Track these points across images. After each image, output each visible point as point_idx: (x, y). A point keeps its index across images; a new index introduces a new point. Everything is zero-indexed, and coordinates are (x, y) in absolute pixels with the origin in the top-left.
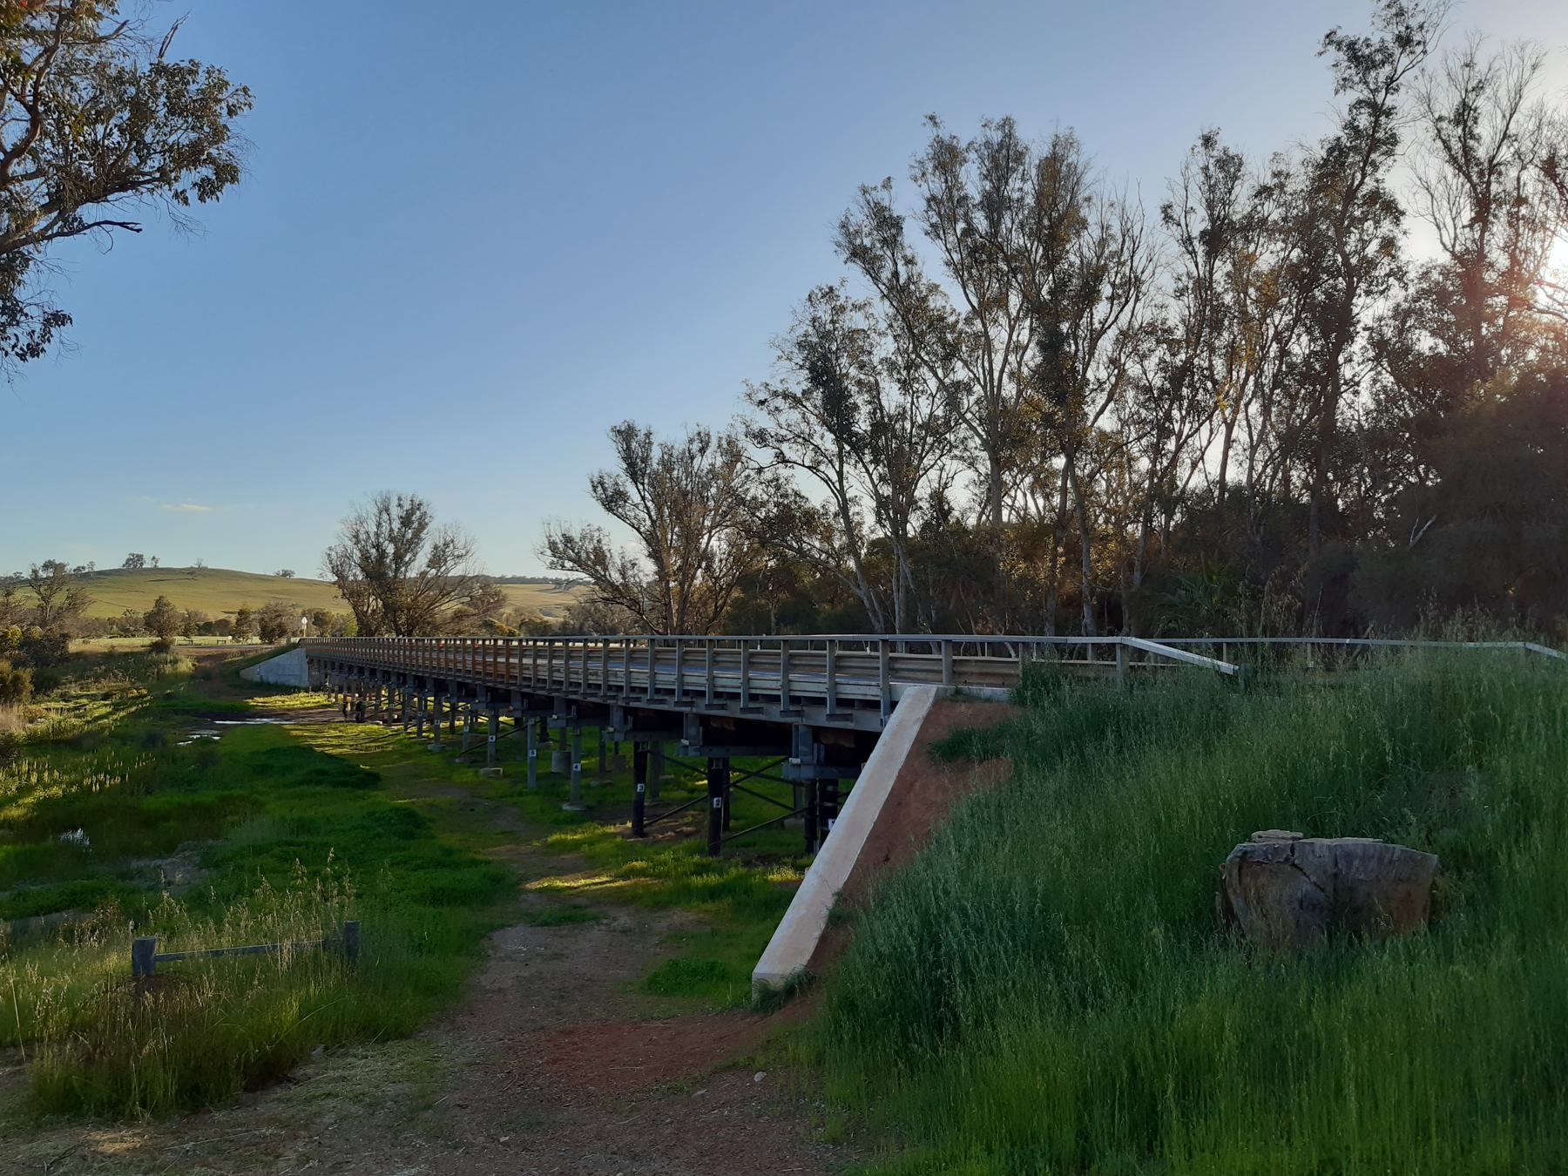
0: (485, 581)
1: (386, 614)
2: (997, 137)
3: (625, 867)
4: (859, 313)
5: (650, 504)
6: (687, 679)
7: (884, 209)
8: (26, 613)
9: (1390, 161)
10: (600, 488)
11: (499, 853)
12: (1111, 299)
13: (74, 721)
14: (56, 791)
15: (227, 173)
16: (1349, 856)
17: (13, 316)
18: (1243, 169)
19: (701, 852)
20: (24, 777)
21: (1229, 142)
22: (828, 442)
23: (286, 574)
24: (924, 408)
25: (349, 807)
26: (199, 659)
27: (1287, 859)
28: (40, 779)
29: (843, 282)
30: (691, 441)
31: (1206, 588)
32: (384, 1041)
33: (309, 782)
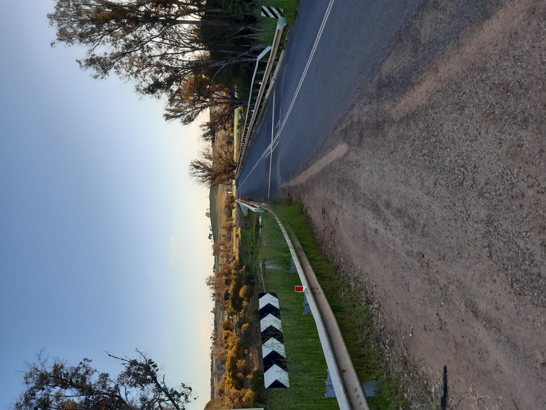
15: (150, 362)
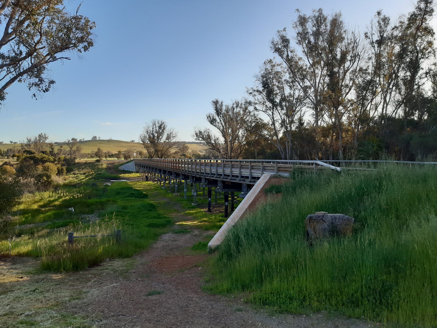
0: (184, 143)
1: (155, 152)
2: (317, 14)
3: (202, 220)
4: (279, 67)
5: (222, 122)
6: (218, 171)
7: (284, 37)
8: (67, 152)
9: (431, 17)
10: (209, 118)
11: (173, 215)
12: (350, 61)
13: (76, 180)
14: (67, 198)
15: (91, 44)
16: (335, 218)
17: (41, 82)
18: (390, 21)
19: (222, 217)
20: (60, 194)
21: (385, 13)
22: (269, 104)
23: (133, 141)
24: (297, 93)
25: (138, 203)
26: (108, 164)
27: (321, 219)
28: (64, 195)
29: (274, 58)
30: (233, 104)
31: (372, 145)
32: (123, 258)
33: (129, 197)
